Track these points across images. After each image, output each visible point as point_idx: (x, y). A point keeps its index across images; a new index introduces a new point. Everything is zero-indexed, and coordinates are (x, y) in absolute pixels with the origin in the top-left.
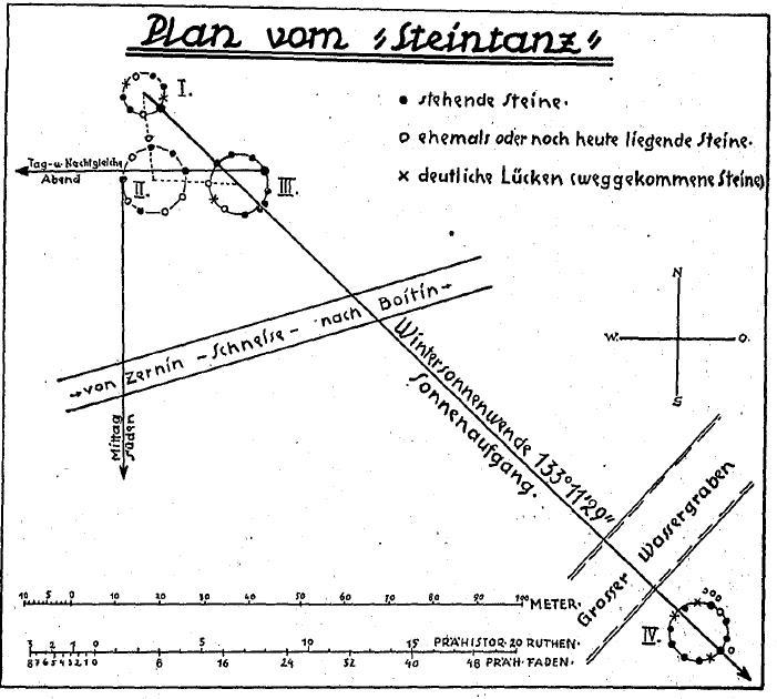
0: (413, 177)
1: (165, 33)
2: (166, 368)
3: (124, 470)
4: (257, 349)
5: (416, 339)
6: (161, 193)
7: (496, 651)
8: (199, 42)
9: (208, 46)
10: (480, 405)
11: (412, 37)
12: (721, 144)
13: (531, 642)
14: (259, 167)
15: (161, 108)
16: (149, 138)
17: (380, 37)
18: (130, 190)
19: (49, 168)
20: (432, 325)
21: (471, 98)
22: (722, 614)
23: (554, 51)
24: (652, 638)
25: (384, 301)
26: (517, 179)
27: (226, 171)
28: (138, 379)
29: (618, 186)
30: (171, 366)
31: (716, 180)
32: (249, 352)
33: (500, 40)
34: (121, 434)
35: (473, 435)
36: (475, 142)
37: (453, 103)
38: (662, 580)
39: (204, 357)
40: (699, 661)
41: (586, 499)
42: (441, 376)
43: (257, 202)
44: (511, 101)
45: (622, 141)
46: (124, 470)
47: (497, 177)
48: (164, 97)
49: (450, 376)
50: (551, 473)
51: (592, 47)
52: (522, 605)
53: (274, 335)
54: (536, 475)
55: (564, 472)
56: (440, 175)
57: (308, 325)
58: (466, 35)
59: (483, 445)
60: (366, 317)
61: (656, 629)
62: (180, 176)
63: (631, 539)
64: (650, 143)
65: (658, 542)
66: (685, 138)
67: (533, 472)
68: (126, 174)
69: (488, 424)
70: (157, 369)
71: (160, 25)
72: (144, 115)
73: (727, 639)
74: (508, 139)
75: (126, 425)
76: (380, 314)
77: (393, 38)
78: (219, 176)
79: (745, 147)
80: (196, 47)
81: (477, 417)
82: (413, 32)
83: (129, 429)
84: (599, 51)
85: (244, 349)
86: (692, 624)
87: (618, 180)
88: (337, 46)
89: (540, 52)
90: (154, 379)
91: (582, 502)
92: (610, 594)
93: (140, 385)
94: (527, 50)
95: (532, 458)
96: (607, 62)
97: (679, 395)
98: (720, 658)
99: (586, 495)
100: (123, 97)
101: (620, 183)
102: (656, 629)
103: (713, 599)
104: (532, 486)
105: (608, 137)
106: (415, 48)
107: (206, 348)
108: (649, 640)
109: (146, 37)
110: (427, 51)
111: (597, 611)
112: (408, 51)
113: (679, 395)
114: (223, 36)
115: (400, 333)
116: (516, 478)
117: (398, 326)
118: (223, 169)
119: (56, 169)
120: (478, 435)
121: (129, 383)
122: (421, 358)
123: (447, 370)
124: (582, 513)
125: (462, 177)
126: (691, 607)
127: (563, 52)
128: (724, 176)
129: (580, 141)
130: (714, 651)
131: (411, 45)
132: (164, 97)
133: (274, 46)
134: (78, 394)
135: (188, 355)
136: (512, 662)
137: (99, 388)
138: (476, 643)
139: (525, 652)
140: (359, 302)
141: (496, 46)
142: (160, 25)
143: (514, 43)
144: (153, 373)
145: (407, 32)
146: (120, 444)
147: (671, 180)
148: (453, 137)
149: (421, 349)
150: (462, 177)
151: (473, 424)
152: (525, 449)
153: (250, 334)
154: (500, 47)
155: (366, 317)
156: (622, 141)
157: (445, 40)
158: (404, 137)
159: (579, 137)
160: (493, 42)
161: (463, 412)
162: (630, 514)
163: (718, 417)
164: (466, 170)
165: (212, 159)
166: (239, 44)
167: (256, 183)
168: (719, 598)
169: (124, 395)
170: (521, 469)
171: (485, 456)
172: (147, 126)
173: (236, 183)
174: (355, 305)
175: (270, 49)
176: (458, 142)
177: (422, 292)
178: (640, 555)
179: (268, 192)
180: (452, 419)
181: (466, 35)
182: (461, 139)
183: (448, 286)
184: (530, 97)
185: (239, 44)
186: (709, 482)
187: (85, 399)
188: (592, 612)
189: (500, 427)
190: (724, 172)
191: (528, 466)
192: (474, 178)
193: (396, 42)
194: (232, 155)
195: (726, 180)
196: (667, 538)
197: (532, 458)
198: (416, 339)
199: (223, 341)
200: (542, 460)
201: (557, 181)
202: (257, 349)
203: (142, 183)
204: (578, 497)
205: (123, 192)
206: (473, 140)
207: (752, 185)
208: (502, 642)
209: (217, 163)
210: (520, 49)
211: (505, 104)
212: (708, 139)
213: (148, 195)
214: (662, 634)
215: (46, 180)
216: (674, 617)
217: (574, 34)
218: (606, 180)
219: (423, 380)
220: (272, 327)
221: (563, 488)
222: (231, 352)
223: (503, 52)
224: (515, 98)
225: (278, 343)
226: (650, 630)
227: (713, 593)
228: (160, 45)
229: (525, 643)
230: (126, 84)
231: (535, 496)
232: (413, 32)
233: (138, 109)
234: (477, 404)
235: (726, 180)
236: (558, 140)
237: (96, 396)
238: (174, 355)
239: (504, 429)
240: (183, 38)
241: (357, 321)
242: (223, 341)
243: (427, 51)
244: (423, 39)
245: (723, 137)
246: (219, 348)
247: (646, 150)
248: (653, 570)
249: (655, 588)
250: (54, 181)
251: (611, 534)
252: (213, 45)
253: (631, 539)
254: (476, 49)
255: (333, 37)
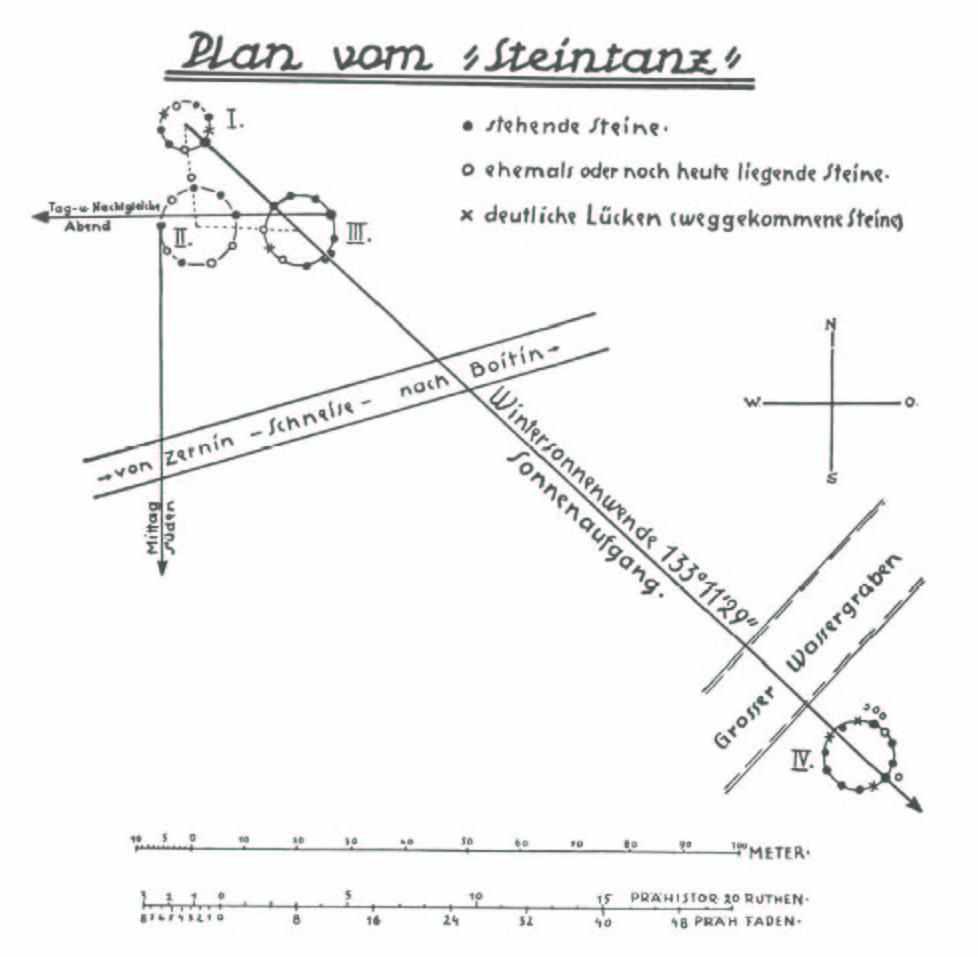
0: (478, 216)
1: (211, 53)
2: (213, 447)
3: (162, 565)
4: (322, 425)
5: (515, 411)
6: (206, 241)
7: (707, 909)
8: (252, 64)
9: (262, 69)
10: (595, 489)
11: (511, 55)
12: (851, 177)
13: (749, 898)
14: (324, 211)
15: (205, 143)
16: (191, 177)
17: (471, 56)
18: (170, 238)
19: (73, 213)
20: (533, 395)
21: (552, 124)
22: (888, 735)
23: (683, 72)
24: (803, 762)
25: (474, 366)
26: (605, 219)
27: (284, 216)
28: (179, 460)
29: (728, 227)
30: (219, 443)
31: (845, 221)
32: (312, 427)
33: (618, 59)
34: (158, 524)
35: (586, 525)
36: (556, 175)
37: (529, 129)
38: (816, 693)
39: (259, 433)
40: (860, 790)
41: (725, 599)
42: (548, 455)
43: (322, 252)
44: (599, 127)
45: (733, 174)
46: (162, 565)
47: (581, 218)
48: (209, 130)
49: (558, 455)
50: (682, 570)
51: (731, 66)
52: (739, 853)
53: (343, 407)
54: (664, 571)
55: (696, 567)
56: (512, 215)
57: (386, 394)
58: (578, 53)
59: (598, 536)
60: (455, 386)
61: (808, 752)
62: (230, 221)
63: (778, 645)
64: (768, 176)
65: (811, 648)
66: (808, 170)
67: (660, 568)
68: (165, 220)
69: (604, 510)
70: (201, 448)
71: (204, 44)
72: (185, 150)
73: (893, 763)
74: (596, 172)
75: (166, 512)
76: (472, 382)
77: (487, 57)
78: (276, 222)
79: (880, 180)
80: (247, 70)
81: (592, 504)
82: (512, 49)
83: (169, 517)
84: (738, 72)
85: (306, 423)
86: (373, 299)
87: (728, 220)
88: (419, 66)
89: (667, 73)
90: (198, 459)
91: (720, 603)
92: (753, 711)
93: (181, 465)
94: (651, 70)
95: (657, 551)
96: (747, 85)
97: (834, 471)
98: (885, 787)
99: (724, 595)
100: (161, 130)
101: (731, 224)
102: (808, 752)
103: (876, 717)
104: (657, 584)
105: (716, 168)
106: (514, 68)
107: (261, 422)
108: (799, 765)
109: (187, 57)
110: (529, 71)
111: (738, 730)
112: (505, 71)
113: (834, 471)
114: (281, 57)
115: (496, 404)
116: (638, 575)
117: (495, 396)
118: (280, 213)
119: (83, 214)
120: (592, 525)
121: (169, 463)
122: (522, 434)
123: (553, 448)
124: (720, 615)
125: (537, 217)
126: (849, 727)
127: (695, 72)
128: (855, 216)
129: (683, 174)
130: (877, 778)
131: (509, 65)
132: (209, 130)
133: (342, 66)
134: (108, 477)
135: (239, 431)
136: (727, 922)
137: (133, 470)
138: (682, 899)
139: (742, 909)
140: (448, 370)
141: (614, 65)
142: (204, 44)
143: (636, 61)
144: (196, 452)
145: (505, 49)
146: (158, 534)
147: (792, 220)
148: (528, 169)
149: (521, 423)
150: (537, 217)
151: (586, 511)
152: (650, 540)
153: (314, 406)
154: (618, 66)
155: (455, 386)
156: (733, 174)
157: (552, 59)
158: (468, 170)
159: (681, 169)
160: (610, 62)
161: (574, 498)
162: (776, 615)
163: (882, 502)
164: (545, 208)
165: (212, 149)
166: (300, 65)
167: (319, 229)
168: (883, 716)
169: (162, 478)
170: (645, 564)
171: (601, 548)
172: (194, 203)
173: (297, 229)
174: (442, 372)
175: (335, 69)
176: (534, 175)
177: (522, 356)
178: (789, 663)
179: (334, 239)
180: (560, 505)
181: (578, 53)
182: (537, 173)
183: (555, 349)
184: (622, 123)
185: (300, 65)
186: (871, 578)
187: (117, 482)
188: (732, 731)
189: (620, 514)
190: (853, 211)
191: (691, 597)
192: (554, 218)
193: (491, 60)
194: (291, 196)
195: (856, 219)
196: (822, 642)
197: (657, 551)
198: (515, 411)
199: (281, 415)
200: (668, 555)
201: (654, 222)
202: (322, 425)
203: (183, 230)
204: (716, 597)
205: (161, 241)
206: (553, 173)
207: (888, 225)
208: (713, 898)
209: (274, 206)
210: (644, 69)
211: (592, 131)
212: (836, 171)
213: (190, 244)
214: (815, 758)
215: (70, 227)
216: (829, 737)
217: (708, 52)
218: (713, 220)
219: (524, 459)
220: (340, 398)
221: (695, 586)
222: (290, 428)
223: (622, 73)
224: (604, 123)
225: (346, 417)
226: (801, 755)
227: (876, 710)
228: (204, 67)
229: (743, 898)
230: (164, 114)
231: (661, 595)
232: (512, 49)
233: (178, 143)
234: (591, 487)
235: (856, 219)
236: (655, 173)
237: (129, 479)
238: (223, 431)
239: (623, 517)
240: (233, 60)
241: (444, 390)
242: (281, 415)
243: (529, 71)
244: (523, 57)
245: (852, 170)
246: (276, 424)
247: (763, 184)
248: (805, 682)
249: (807, 704)
250: (80, 228)
251: (754, 639)
252: (268, 66)
253: (778, 645)
254: (590, 68)
255: (414, 57)
